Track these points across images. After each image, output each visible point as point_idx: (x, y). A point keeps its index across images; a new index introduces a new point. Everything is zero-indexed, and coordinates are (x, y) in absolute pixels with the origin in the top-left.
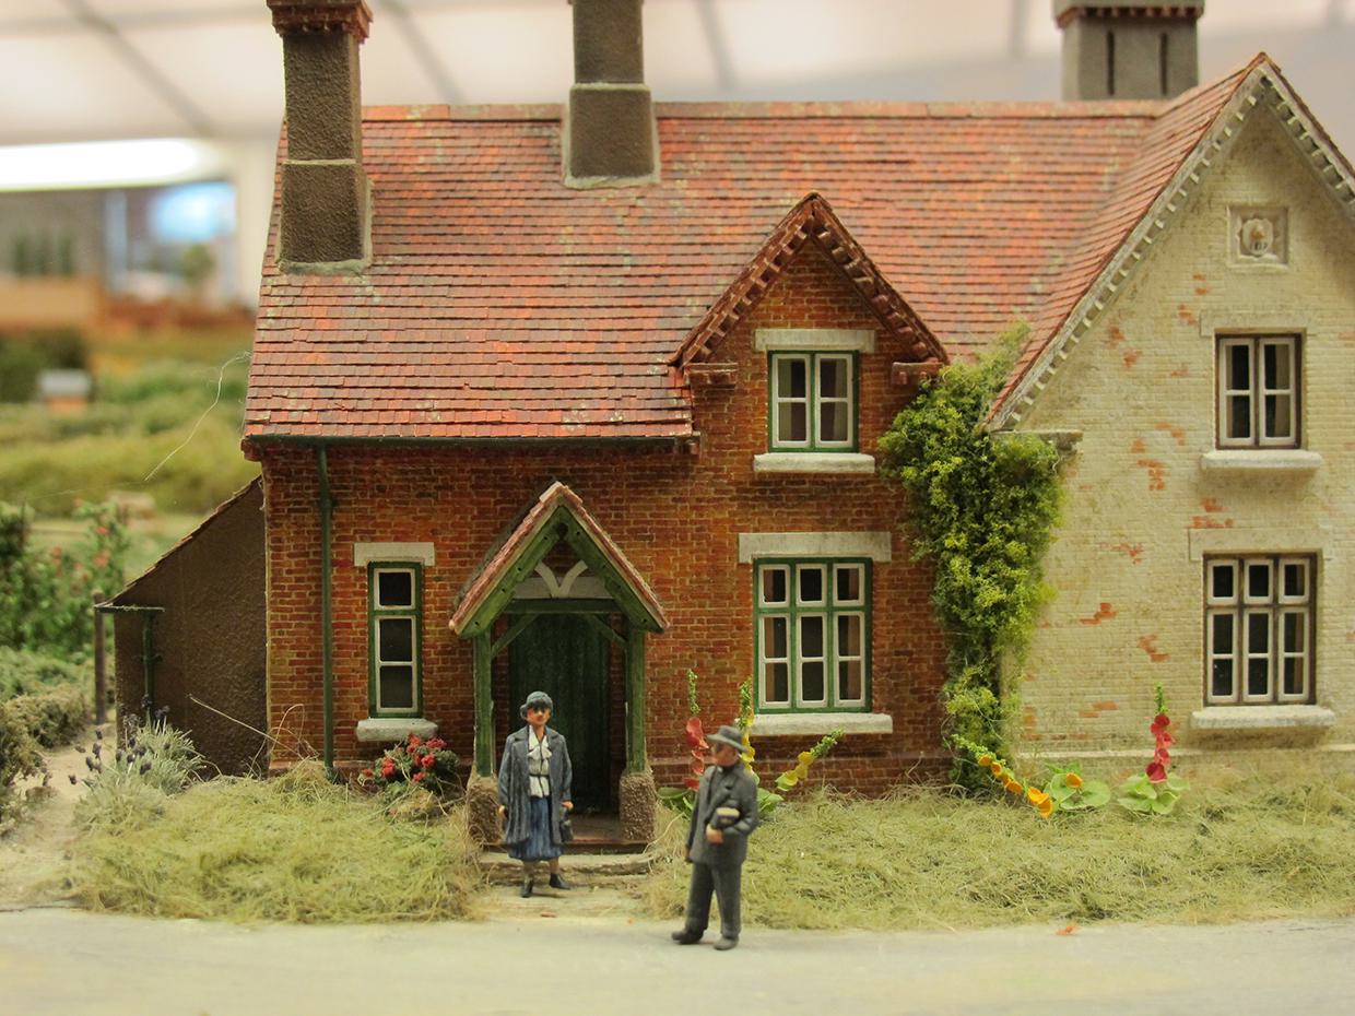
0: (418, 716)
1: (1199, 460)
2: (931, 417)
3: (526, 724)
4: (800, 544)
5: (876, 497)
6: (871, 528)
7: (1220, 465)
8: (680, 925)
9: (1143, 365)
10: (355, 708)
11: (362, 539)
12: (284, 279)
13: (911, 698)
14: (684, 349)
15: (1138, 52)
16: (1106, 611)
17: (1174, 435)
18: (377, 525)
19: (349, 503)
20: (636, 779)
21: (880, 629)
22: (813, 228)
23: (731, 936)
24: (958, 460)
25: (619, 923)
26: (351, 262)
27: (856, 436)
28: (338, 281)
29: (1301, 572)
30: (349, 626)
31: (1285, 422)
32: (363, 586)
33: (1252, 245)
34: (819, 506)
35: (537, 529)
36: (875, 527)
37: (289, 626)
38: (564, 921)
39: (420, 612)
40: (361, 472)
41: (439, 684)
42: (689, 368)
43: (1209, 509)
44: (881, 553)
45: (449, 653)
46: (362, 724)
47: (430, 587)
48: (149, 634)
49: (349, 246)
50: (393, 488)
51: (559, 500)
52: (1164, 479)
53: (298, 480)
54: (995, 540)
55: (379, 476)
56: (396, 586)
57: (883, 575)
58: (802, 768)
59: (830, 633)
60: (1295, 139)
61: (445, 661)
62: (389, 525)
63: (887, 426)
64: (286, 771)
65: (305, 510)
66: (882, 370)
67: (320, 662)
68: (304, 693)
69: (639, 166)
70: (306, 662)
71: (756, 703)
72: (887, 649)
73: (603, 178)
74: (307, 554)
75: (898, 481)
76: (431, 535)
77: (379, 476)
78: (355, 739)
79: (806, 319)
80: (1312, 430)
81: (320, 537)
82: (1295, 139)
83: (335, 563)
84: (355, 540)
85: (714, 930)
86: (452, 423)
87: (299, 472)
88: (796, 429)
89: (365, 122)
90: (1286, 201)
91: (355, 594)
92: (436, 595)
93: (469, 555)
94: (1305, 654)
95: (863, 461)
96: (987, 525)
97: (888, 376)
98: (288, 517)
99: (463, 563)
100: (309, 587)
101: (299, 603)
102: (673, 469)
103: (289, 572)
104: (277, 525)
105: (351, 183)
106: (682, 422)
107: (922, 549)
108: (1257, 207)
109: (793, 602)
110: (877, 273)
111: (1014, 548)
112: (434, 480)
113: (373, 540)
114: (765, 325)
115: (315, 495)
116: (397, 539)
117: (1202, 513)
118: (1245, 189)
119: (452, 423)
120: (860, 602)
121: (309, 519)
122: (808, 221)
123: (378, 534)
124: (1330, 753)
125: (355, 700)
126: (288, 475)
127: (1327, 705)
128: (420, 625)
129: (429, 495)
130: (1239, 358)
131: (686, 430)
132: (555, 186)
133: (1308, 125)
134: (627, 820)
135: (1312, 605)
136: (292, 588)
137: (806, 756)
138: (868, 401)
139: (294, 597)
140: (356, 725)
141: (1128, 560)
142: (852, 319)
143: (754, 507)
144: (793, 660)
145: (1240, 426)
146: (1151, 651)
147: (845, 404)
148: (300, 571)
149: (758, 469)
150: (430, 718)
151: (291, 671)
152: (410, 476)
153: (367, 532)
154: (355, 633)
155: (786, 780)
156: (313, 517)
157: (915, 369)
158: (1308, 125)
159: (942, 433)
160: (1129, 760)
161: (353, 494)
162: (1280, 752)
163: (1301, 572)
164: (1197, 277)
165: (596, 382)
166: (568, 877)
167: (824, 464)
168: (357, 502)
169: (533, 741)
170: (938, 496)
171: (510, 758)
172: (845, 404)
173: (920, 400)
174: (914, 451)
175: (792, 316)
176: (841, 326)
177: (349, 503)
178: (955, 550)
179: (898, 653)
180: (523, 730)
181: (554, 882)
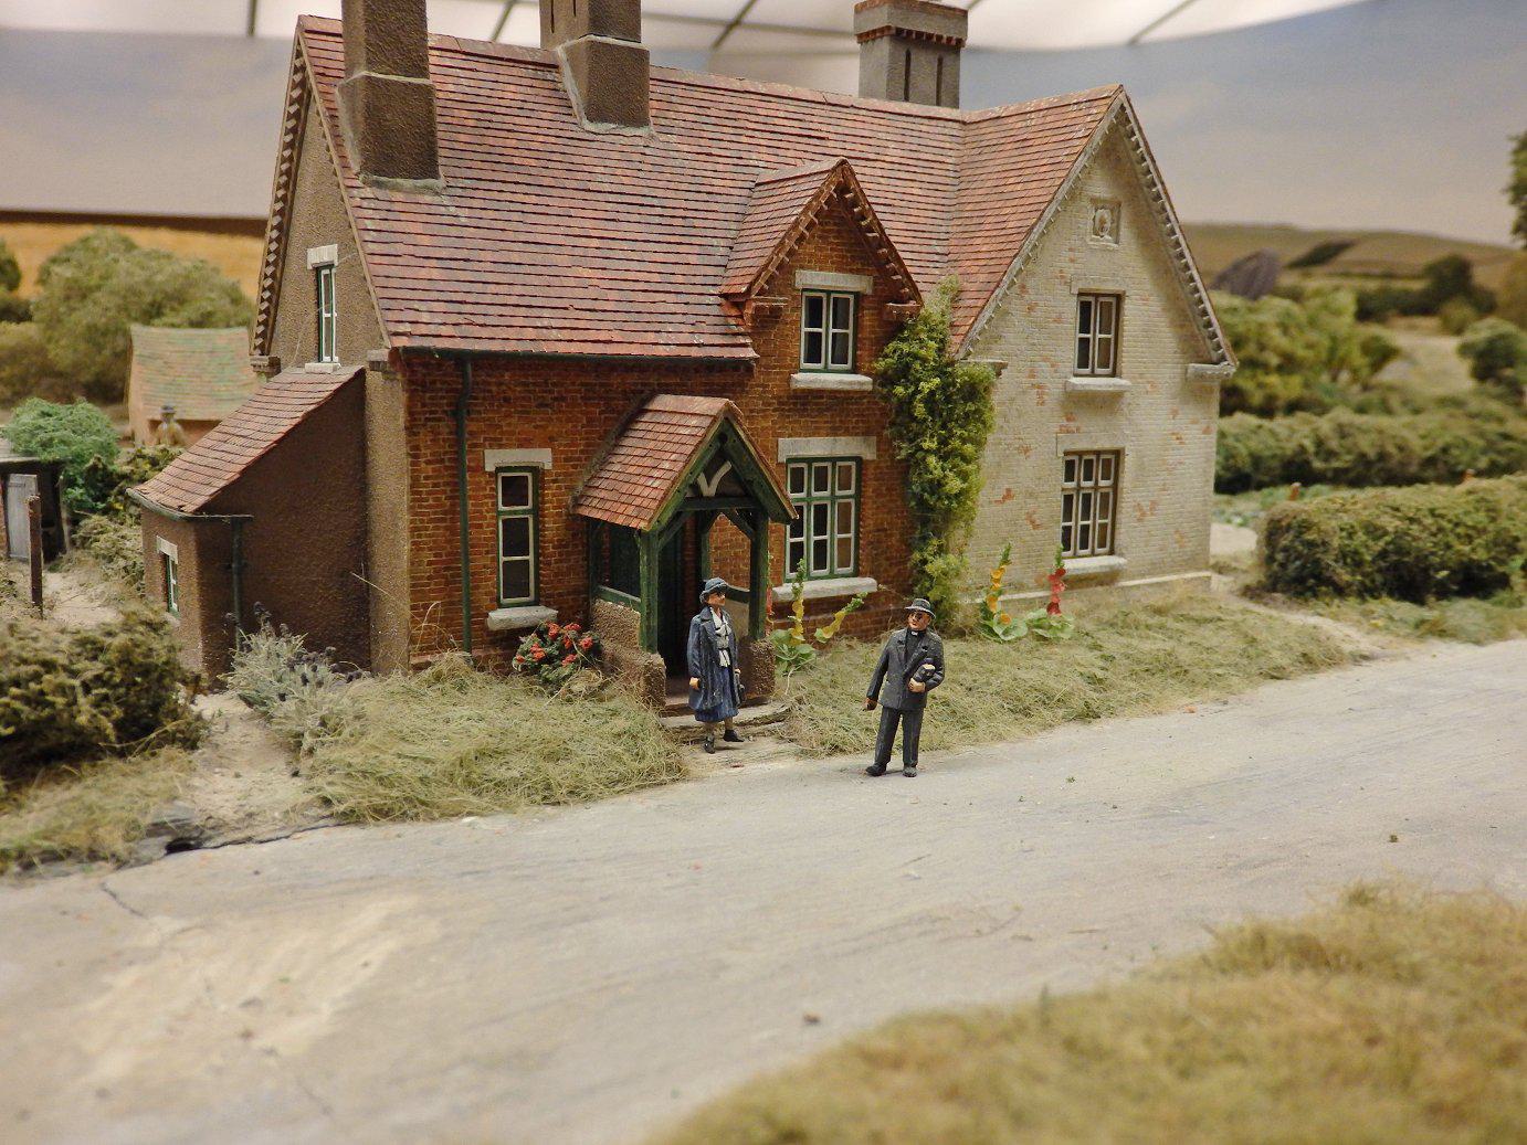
0: (536, 603)
1: (1065, 385)
2: (915, 348)
3: (708, 606)
4: (817, 446)
5: (868, 409)
6: (863, 434)
7: (1080, 388)
8: (870, 760)
9: (1038, 313)
10: (486, 601)
11: (491, 447)
12: (368, 192)
13: (885, 563)
14: (751, 284)
15: (924, 64)
16: (1009, 495)
17: (1053, 366)
18: (502, 433)
19: (479, 412)
20: (763, 644)
21: (868, 512)
22: (843, 189)
23: (911, 758)
24: (937, 380)
25: (786, 765)
26: (430, 181)
27: (854, 361)
28: (420, 198)
29: (1112, 462)
30: (480, 526)
31: (1109, 361)
32: (492, 489)
33: (1099, 230)
34: (832, 416)
35: (709, 438)
36: (867, 433)
37: (426, 529)
38: (753, 769)
39: (537, 512)
40: (489, 384)
41: (556, 575)
42: (755, 300)
43: (1068, 420)
44: (869, 454)
45: (565, 546)
46: (492, 615)
47: (549, 488)
48: (239, 542)
49: (425, 164)
50: (517, 399)
51: (725, 412)
52: (1045, 397)
53: (433, 391)
54: (956, 443)
55: (504, 388)
56: (514, 488)
57: (871, 471)
58: (837, 624)
59: (832, 518)
60: (1132, 153)
61: (560, 554)
62: (513, 433)
63: (879, 353)
64: (428, 664)
65: (439, 420)
66: (875, 308)
67: (458, 561)
68: (441, 591)
69: (641, 121)
70: (442, 562)
71: (808, 574)
72: (871, 528)
73: (612, 126)
74: (442, 461)
75: (890, 394)
76: (548, 441)
77: (504, 388)
78: (485, 629)
79: (829, 265)
80: (1126, 362)
81: (458, 442)
82: (1132, 153)
83: (470, 469)
84: (485, 447)
85: (896, 761)
86: (572, 341)
87: (434, 382)
88: (814, 355)
89: (432, 48)
90: (1120, 198)
91: (485, 497)
92: (554, 495)
93: (579, 459)
94: (1108, 521)
95: (862, 381)
96: (951, 430)
97: (880, 314)
98: (424, 425)
99: (575, 467)
100: (444, 492)
101: (437, 506)
102: (733, 385)
103: (426, 478)
104: (415, 434)
105: (430, 103)
106: (745, 345)
107: (904, 450)
108: (1105, 201)
109: (809, 493)
110: (882, 231)
111: (969, 448)
112: (551, 392)
113: (501, 446)
114: (802, 267)
115: (449, 405)
116: (521, 446)
117: (1065, 423)
118: (1100, 187)
119: (572, 341)
120: (851, 492)
121: (445, 428)
122: (840, 183)
123: (504, 442)
124: (1123, 588)
125: (486, 594)
126: (423, 384)
127: (1121, 555)
128: (536, 523)
129: (547, 405)
130: (1085, 309)
131: (750, 353)
132: (574, 127)
133: (1142, 144)
134: (756, 679)
135: (1115, 487)
136: (428, 493)
137: (842, 613)
138: (865, 334)
139: (431, 502)
140: (487, 616)
141: (1022, 457)
142: (859, 266)
143: (788, 417)
144: (808, 539)
145: (1083, 361)
146: (1033, 522)
147: (846, 335)
148: (436, 477)
149: (794, 386)
150: (548, 605)
151: (430, 570)
152: (532, 388)
153: (495, 439)
154: (485, 533)
155: (822, 634)
156: (448, 426)
157: (901, 309)
158: (1142, 144)
159: (924, 360)
160: (1019, 600)
161: (482, 404)
162: (1100, 589)
163: (1112, 462)
164: (1071, 250)
165: (673, 308)
166: (738, 731)
167: (841, 382)
168: (486, 411)
169: (717, 619)
170: (920, 410)
171: (699, 637)
172: (846, 335)
173: (906, 333)
174: (903, 372)
175: (819, 261)
176: (851, 271)
177: (479, 412)
178: (928, 451)
179: (878, 530)
180: (705, 610)
181: (730, 736)
